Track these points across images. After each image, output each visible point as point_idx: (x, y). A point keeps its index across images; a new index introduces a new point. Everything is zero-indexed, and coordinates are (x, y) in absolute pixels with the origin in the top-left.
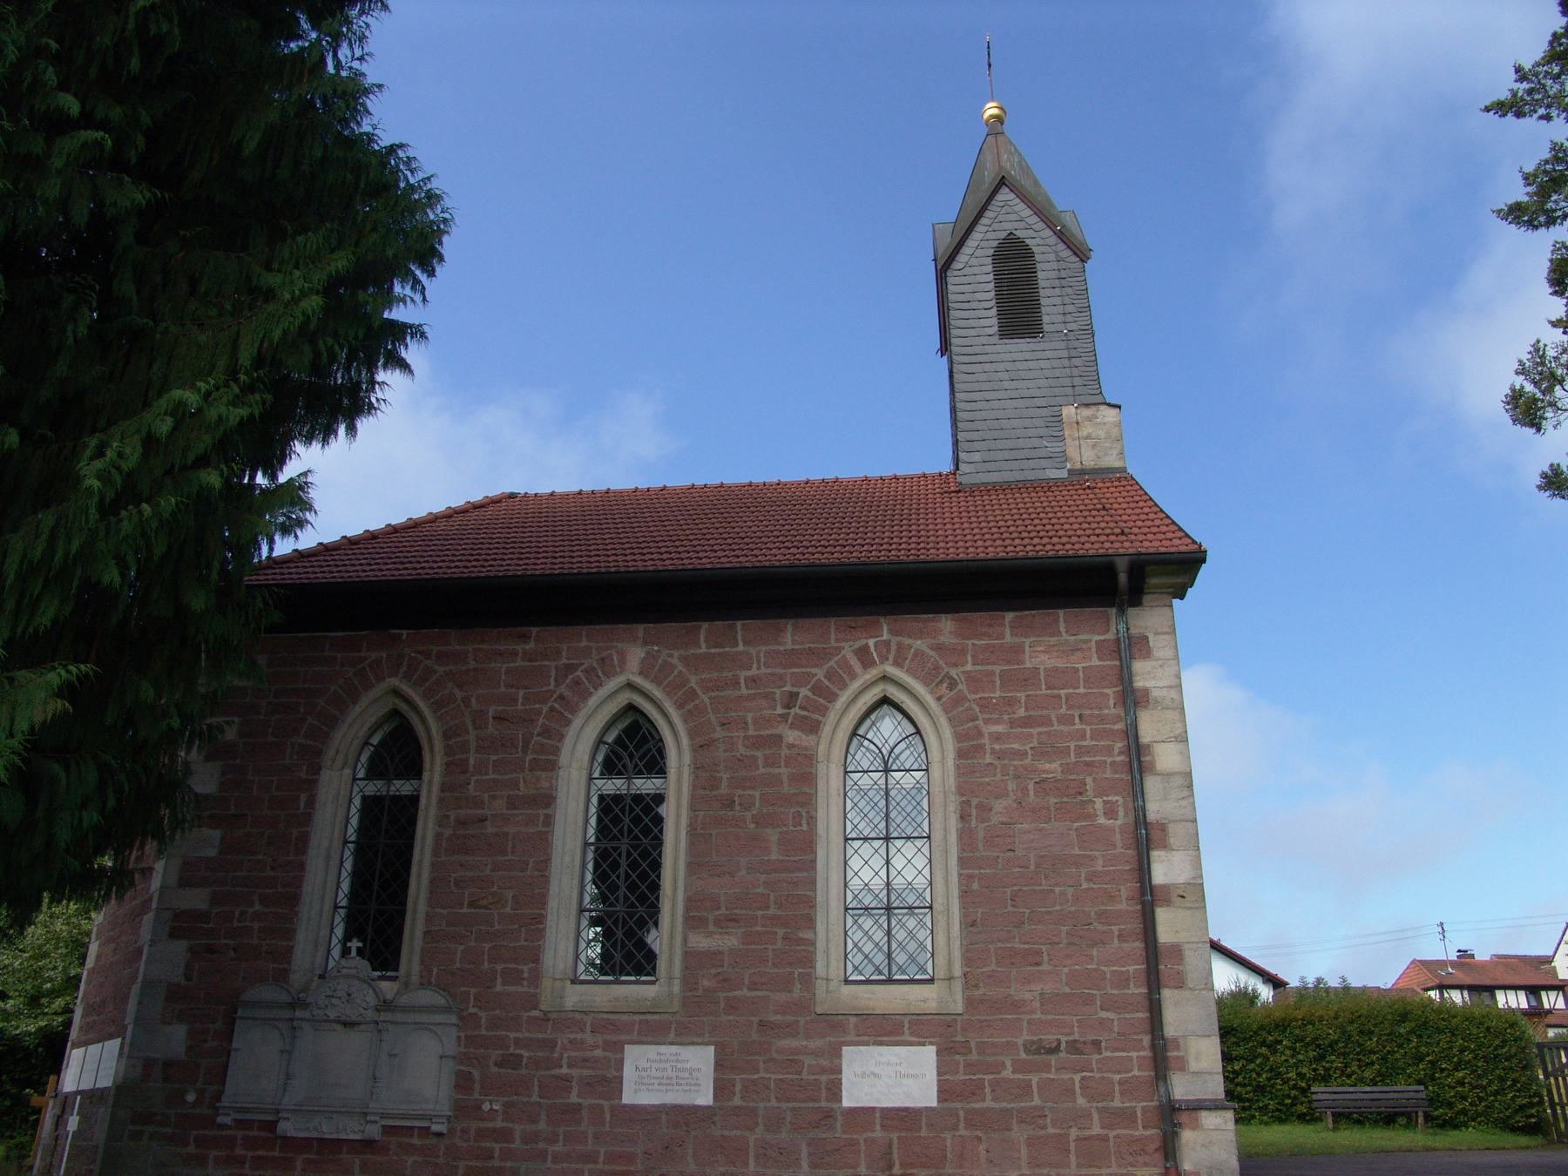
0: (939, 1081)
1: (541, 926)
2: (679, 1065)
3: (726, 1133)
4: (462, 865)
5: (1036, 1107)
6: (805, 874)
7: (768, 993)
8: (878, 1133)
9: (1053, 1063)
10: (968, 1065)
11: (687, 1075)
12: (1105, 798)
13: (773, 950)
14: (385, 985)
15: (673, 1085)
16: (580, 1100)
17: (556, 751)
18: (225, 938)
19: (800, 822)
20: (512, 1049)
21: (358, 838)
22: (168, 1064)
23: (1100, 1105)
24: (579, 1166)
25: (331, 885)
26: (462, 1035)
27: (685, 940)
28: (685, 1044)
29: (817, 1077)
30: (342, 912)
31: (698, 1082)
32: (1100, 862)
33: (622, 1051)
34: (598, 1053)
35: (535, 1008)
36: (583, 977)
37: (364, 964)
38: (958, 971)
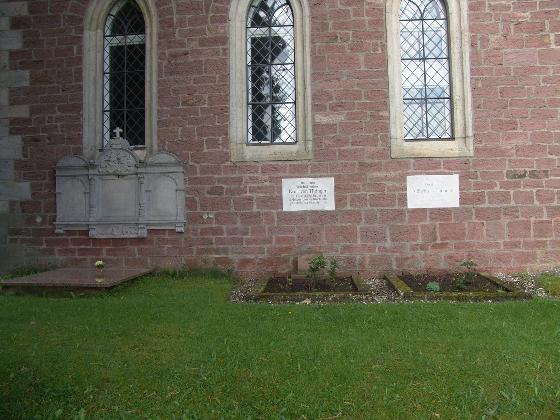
0: (460, 193)
1: (227, 114)
2: (314, 189)
3: (344, 225)
4: (176, 81)
5: (513, 207)
6: (381, 79)
7: (363, 147)
8: (428, 222)
9: (522, 183)
10: (476, 184)
11: (319, 194)
12: (556, 33)
13: (365, 122)
14: (138, 153)
15: (311, 200)
16: (259, 210)
17: (227, 11)
18: (42, 133)
19: (377, 48)
20: (216, 184)
21: (111, 70)
22: (22, 203)
23: (547, 205)
24: (262, 246)
25: (99, 97)
26: (187, 178)
27: (313, 118)
28: (317, 177)
29: (393, 193)
30: (108, 113)
31: (326, 198)
32: (551, 71)
33: (281, 182)
34: (267, 184)
35: (228, 161)
36: (252, 142)
37: (125, 142)
38: (470, 132)
